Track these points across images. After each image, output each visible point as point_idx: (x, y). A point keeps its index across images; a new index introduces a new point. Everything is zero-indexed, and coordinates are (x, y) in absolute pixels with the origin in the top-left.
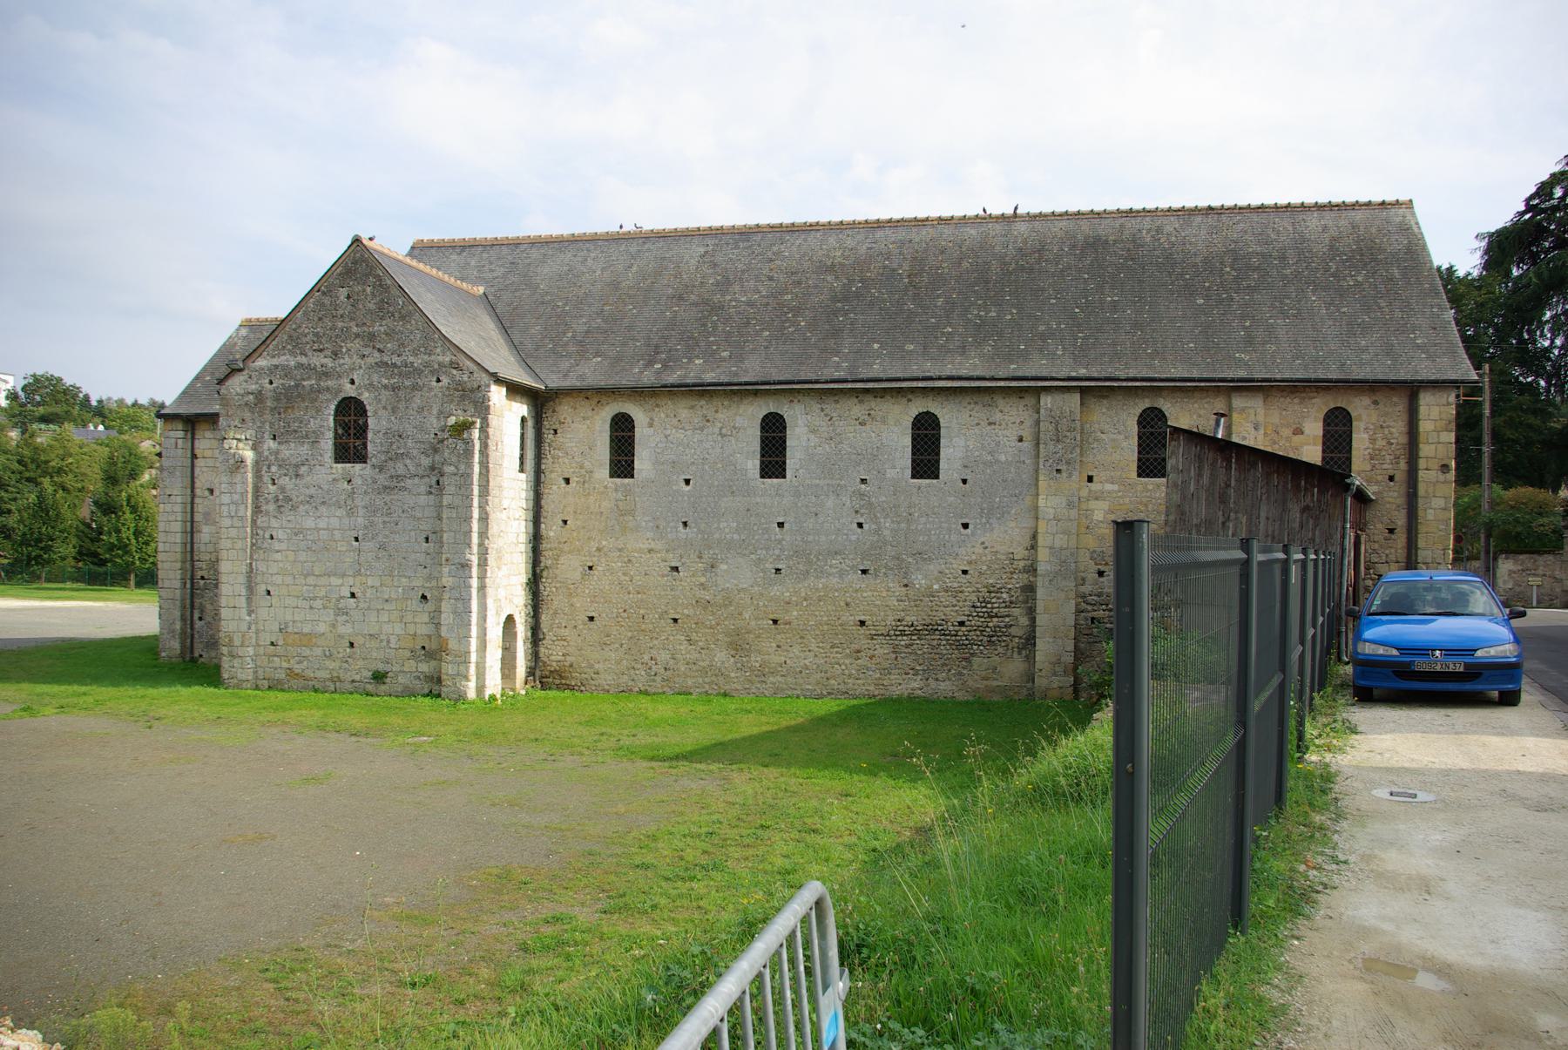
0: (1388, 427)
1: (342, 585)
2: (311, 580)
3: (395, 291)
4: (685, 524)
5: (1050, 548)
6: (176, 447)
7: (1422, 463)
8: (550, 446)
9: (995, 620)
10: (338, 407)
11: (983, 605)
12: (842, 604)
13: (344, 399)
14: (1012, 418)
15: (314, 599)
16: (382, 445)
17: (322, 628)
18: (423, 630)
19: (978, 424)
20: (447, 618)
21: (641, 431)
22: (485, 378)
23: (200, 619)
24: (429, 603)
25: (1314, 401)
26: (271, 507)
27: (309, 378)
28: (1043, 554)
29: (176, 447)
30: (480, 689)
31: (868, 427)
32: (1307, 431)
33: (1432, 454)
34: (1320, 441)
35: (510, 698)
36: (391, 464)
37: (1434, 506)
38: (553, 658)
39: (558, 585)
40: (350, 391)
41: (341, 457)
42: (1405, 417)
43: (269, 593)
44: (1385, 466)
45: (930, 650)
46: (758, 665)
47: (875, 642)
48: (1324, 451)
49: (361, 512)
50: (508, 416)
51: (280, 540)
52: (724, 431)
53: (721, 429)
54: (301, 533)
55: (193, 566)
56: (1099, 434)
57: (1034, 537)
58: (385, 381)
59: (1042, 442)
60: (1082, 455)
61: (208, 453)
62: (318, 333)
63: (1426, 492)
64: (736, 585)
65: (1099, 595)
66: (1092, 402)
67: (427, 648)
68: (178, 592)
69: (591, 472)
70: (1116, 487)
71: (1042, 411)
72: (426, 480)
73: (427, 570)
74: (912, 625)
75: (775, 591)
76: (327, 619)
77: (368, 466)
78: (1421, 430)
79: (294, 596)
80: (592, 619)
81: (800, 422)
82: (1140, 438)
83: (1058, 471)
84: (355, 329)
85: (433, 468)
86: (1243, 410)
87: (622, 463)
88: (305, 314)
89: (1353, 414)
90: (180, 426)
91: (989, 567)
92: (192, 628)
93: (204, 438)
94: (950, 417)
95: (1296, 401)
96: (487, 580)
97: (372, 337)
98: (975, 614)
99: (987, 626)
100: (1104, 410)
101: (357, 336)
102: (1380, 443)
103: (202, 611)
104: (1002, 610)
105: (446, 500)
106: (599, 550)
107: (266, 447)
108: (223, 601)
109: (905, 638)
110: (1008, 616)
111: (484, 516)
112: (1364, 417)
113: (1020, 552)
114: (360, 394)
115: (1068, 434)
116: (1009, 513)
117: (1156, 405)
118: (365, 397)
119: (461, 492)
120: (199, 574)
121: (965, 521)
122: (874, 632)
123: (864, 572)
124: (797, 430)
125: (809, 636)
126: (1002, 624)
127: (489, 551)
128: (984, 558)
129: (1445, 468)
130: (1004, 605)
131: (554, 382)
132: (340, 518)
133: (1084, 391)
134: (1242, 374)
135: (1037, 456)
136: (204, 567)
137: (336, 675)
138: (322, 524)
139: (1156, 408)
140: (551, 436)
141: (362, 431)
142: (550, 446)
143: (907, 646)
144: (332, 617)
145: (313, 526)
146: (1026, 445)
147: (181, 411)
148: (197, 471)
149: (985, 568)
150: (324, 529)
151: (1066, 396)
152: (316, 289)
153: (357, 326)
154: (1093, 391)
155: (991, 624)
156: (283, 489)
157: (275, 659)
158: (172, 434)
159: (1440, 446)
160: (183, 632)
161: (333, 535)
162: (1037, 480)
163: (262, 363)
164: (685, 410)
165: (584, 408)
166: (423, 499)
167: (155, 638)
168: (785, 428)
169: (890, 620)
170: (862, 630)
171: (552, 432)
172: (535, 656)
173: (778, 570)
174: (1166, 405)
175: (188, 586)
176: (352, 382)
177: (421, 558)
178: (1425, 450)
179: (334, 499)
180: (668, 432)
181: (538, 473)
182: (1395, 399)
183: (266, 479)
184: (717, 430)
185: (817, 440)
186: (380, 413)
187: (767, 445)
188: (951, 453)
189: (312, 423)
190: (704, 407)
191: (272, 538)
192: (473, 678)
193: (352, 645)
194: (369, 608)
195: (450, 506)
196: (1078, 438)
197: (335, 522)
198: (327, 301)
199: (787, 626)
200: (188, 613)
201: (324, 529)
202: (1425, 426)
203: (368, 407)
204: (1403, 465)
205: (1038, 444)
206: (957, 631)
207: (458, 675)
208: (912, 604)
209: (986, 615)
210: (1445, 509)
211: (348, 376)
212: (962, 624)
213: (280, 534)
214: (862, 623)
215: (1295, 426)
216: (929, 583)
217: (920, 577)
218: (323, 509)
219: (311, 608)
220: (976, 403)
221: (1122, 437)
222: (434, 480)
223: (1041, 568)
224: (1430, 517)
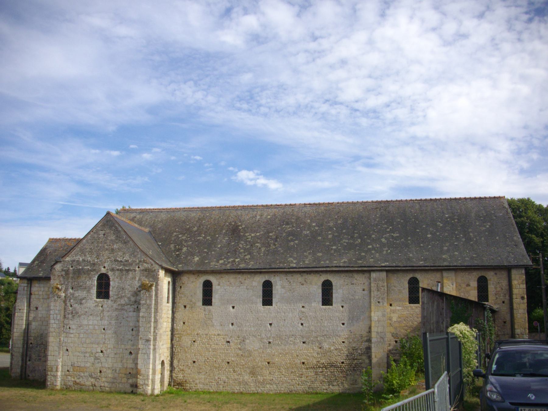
0: (501, 283)
1: (98, 347)
2: (85, 346)
3: (123, 233)
4: (232, 324)
5: (377, 332)
6: (24, 290)
7: (514, 296)
8: (178, 293)
9: (356, 361)
10: (98, 277)
11: (351, 355)
12: (295, 355)
13: (101, 274)
14: (360, 280)
15: (86, 353)
16: (115, 292)
17: (88, 365)
18: (131, 365)
19: (347, 284)
20: (140, 361)
21: (215, 287)
22: (157, 267)
23: (29, 360)
24: (133, 355)
25: (473, 273)
26: (70, 316)
27: (87, 266)
28: (374, 335)
29: (24, 290)
30: (153, 389)
31: (304, 286)
32: (471, 285)
33: (518, 293)
34: (476, 289)
35: (163, 394)
36: (119, 300)
37: (520, 312)
38: (178, 378)
39: (181, 348)
40: (103, 271)
41: (99, 297)
42: (507, 279)
43: (67, 350)
44: (501, 298)
45: (330, 374)
46: (262, 381)
47: (309, 371)
48: (478, 292)
49: (107, 318)
50: (165, 281)
51: (73, 329)
52: (248, 287)
53: (247, 286)
54: (82, 326)
55: (28, 339)
56: (394, 287)
57: (370, 328)
58: (118, 268)
59: (372, 291)
60: (387, 296)
61: (36, 293)
62: (91, 248)
63: (517, 307)
64: (253, 348)
65: (396, 350)
66: (390, 275)
67: (131, 373)
68: (21, 350)
69: (195, 303)
70: (401, 308)
71: (372, 279)
72: (133, 306)
73: (132, 342)
74: (323, 364)
75: (269, 351)
76: (91, 361)
77: (109, 301)
78: (513, 283)
79: (78, 352)
80: (194, 362)
81: (278, 284)
82: (409, 289)
83: (379, 302)
84: (106, 247)
85: (136, 302)
86: (447, 277)
87: (207, 300)
88: (87, 241)
89: (488, 278)
90: (26, 281)
91: (353, 340)
92: (26, 364)
93: (35, 287)
94: (336, 281)
95: (467, 274)
96: (156, 346)
97: (113, 249)
98: (348, 359)
99: (353, 364)
100: (395, 278)
101: (107, 249)
102: (499, 289)
103: (30, 357)
104: (358, 357)
105: (141, 314)
106: (197, 334)
107: (69, 292)
108: (49, 353)
109: (320, 369)
110: (361, 359)
111: (156, 321)
112: (492, 279)
113: (364, 333)
114: (108, 272)
115: (382, 288)
116: (360, 318)
117: (415, 276)
118: (110, 274)
119: (147, 311)
120: (30, 342)
121: (343, 322)
122: (308, 367)
123: (304, 343)
124: (277, 287)
125: (282, 369)
126: (358, 363)
127: (158, 335)
128: (351, 337)
129: (523, 298)
130: (359, 355)
131: (180, 267)
132: (97, 320)
133: (387, 271)
134: (446, 264)
135: (370, 296)
136: (32, 339)
137: (93, 384)
138: (91, 323)
139: (415, 277)
140: (179, 289)
141: (108, 285)
142: (178, 293)
143: (321, 372)
144: (93, 360)
145: (87, 323)
146: (366, 292)
147: (26, 276)
148: (32, 300)
149: (351, 340)
150: (91, 325)
151: (381, 273)
152: (92, 231)
153: (107, 246)
154: (391, 271)
155: (354, 363)
156: (75, 309)
157: (69, 377)
158: (23, 285)
159: (520, 289)
160: (22, 366)
161: (94, 327)
162: (370, 306)
163: (68, 259)
164: (232, 278)
165: (192, 278)
166: (131, 314)
167: (8, 368)
168: (272, 286)
169: (315, 362)
170: (303, 366)
171: (179, 287)
172: (171, 376)
173: (270, 343)
174: (418, 276)
175: (25, 346)
176: (104, 267)
177: (130, 337)
178: (515, 291)
179: (96, 313)
180: (226, 288)
181: (174, 303)
182: (503, 272)
183: (68, 304)
184: (245, 287)
185: (285, 291)
186: (115, 280)
187: (265, 293)
188: (337, 295)
189: (88, 283)
190: (241, 277)
191: (70, 328)
192: (150, 386)
193: (101, 372)
194: (108, 357)
195: (143, 317)
196: (386, 289)
197: (96, 322)
198: (96, 236)
199: (274, 365)
200: (25, 358)
201: (91, 325)
202: (515, 283)
203: (110, 277)
204: (507, 297)
205: (370, 292)
206: (341, 366)
207: (144, 384)
208: (323, 355)
209: (352, 359)
210: (524, 314)
211: (103, 265)
212: (343, 363)
213: (73, 327)
214: (303, 363)
215: (467, 283)
216: (329, 347)
217: (326, 344)
218: (91, 317)
219: (84, 356)
220: (346, 276)
221: (402, 289)
222: (136, 306)
223: (373, 340)
224: (519, 317)
